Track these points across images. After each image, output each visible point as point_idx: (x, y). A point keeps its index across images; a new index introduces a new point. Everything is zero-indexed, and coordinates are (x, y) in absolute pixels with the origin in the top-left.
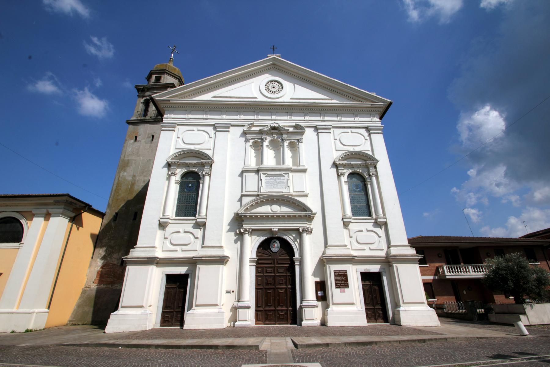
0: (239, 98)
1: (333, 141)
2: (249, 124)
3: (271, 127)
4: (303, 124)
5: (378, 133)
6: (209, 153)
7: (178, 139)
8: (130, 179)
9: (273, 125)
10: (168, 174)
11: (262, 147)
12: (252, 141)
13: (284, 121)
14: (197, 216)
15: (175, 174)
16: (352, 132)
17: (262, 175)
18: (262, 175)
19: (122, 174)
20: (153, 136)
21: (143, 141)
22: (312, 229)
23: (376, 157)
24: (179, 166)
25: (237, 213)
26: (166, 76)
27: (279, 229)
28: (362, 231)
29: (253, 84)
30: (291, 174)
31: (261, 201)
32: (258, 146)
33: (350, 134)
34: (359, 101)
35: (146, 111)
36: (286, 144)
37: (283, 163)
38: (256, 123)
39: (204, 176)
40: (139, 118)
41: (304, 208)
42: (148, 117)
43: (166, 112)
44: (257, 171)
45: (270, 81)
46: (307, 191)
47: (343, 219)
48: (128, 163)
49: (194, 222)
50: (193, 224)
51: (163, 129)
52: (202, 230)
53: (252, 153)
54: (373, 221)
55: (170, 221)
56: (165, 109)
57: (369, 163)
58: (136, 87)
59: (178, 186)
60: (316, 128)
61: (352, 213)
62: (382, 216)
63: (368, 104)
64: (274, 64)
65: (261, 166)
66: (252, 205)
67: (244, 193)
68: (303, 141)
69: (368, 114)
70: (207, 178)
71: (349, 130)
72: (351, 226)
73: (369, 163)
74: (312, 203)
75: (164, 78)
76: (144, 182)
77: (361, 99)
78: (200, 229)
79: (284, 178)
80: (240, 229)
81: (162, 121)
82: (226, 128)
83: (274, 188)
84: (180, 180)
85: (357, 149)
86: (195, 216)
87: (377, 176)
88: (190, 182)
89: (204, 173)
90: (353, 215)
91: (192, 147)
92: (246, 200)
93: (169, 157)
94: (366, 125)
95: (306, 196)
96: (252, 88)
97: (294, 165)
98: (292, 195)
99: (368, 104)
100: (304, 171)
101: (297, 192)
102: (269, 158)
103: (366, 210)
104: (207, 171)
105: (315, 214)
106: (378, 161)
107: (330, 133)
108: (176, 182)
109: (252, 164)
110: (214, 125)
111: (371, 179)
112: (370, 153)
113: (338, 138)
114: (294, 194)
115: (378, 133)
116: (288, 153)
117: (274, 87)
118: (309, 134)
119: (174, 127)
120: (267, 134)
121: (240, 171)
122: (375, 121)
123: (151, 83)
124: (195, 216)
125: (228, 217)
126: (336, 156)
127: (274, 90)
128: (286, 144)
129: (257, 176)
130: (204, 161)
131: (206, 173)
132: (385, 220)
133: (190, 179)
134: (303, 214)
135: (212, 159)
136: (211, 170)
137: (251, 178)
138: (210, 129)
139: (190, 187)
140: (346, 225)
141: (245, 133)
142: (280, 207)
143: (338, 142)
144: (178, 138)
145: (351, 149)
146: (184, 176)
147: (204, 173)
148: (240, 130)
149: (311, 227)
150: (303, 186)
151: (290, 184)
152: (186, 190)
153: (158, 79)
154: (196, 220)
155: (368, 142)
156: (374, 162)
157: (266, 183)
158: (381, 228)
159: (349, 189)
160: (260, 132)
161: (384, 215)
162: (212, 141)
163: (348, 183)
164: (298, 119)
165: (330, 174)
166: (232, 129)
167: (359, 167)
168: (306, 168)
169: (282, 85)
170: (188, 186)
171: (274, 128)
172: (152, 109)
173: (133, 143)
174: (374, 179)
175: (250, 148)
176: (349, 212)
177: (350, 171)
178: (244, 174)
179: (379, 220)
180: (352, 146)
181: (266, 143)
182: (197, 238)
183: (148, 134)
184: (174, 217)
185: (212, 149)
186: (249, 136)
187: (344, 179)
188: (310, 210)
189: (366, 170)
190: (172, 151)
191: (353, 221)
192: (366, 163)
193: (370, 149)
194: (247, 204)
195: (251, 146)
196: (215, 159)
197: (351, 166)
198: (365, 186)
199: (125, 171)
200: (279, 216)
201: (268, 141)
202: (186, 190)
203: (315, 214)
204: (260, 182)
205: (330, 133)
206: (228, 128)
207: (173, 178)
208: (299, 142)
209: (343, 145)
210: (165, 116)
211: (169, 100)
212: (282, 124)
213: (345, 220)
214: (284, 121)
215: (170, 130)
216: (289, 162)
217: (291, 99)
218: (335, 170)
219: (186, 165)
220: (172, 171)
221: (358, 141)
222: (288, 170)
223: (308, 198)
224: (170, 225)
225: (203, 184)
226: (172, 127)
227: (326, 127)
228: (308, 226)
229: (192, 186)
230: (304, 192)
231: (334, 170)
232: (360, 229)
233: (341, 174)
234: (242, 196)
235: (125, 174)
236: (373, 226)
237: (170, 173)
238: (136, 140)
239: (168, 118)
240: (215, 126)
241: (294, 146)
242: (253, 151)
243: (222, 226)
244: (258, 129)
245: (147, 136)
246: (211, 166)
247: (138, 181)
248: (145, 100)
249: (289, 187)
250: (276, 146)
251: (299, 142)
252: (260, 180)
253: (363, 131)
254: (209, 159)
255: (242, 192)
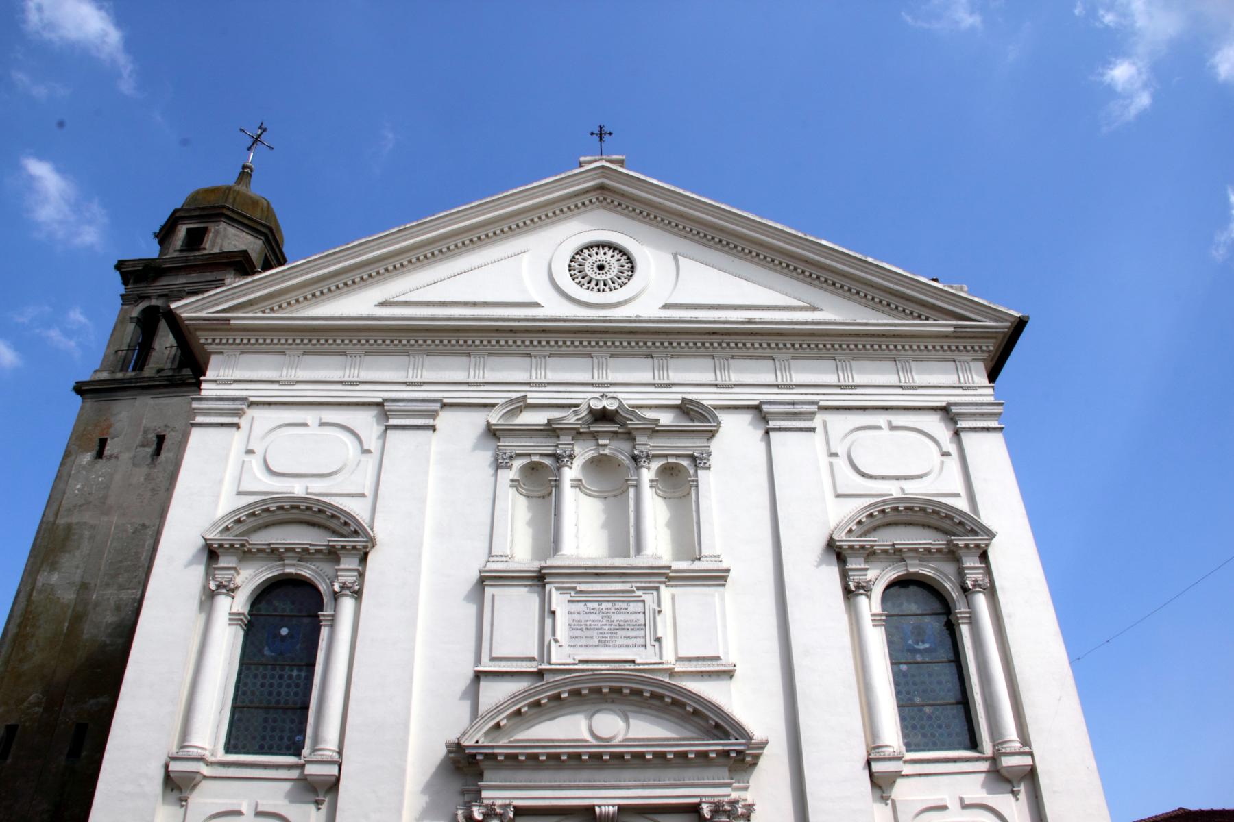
0: (474, 305)
1: (824, 460)
2: (511, 401)
3: (591, 411)
4: (708, 398)
5: (988, 429)
6: (358, 509)
7: (248, 458)
8: (68, 596)
9: (597, 405)
10: (205, 587)
11: (557, 484)
12: (518, 464)
13: (633, 385)
14: (306, 752)
15: (231, 591)
16: (893, 428)
17: (555, 594)
18: (555, 594)
19: (41, 579)
20: (161, 439)
21: (125, 457)
22: (750, 808)
23: (987, 518)
24: (246, 554)
25: (458, 745)
26: (222, 226)
27: (622, 809)
28: (944, 808)
29: (526, 257)
30: (666, 592)
31: (551, 698)
32: (541, 481)
33: (886, 432)
34: (919, 317)
35: (145, 347)
36: (648, 474)
37: (639, 550)
38: (534, 397)
39: (336, 596)
40: (119, 375)
41: (717, 724)
42: (148, 372)
43: (214, 360)
44: (539, 579)
45: (589, 247)
46: (731, 657)
47: (869, 763)
48: (67, 538)
49: (295, 774)
50: (287, 786)
51: (199, 419)
52: (324, 807)
53: (516, 511)
54: (984, 766)
55: (205, 770)
56: (210, 348)
57: (960, 541)
58: (120, 266)
59: (241, 633)
60: (759, 411)
61: (905, 736)
62: (1017, 745)
63: (945, 325)
64: (602, 188)
65: (550, 563)
66: (518, 713)
67: (487, 666)
68: (713, 461)
69: (945, 360)
70: (347, 604)
71: (881, 419)
72: (901, 790)
73: (960, 541)
74: (750, 704)
75: (217, 232)
76: (118, 608)
77: (917, 310)
78: (318, 803)
79: (639, 607)
80: (468, 807)
81: (198, 385)
82: (422, 415)
83: (603, 644)
84: (246, 610)
85: (915, 489)
86: (298, 754)
87: (991, 592)
88: (284, 619)
89: (337, 587)
90: (909, 747)
91: (298, 489)
92: (495, 694)
93: (215, 525)
94: (941, 401)
95: (729, 674)
96: (523, 274)
97: (678, 557)
98: (671, 673)
99: (945, 325)
100: (718, 578)
101: (690, 659)
102: (584, 530)
103: (958, 725)
104: (349, 578)
105: (763, 745)
106: (991, 535)
107: (813, 430)
108: (234, 618)
109: (520, 552)
110: (757, 409)
111: (970, 604)
112: (962, 504)
113: (841, 450)
114: (679, 668)
115: (988, 429)
116: (655, 510)
117: (601, 267)
118: (736, 438)
119: (239, 413)
120: (577, 434)
121: (475, 576)
122: (966, 382)
123: (172, 254)
124: (298, 754)
125: (421, 754)
126: (838, 516)
127: (601, 277)
128: (648, 474)
129: (534, 600)
130: (338, 542)
131: (344, 587)
132: (1027, 761)
133: (282, 605)
134: (714, 747)
135: (366, 534)
136: (361, 575)
137: (515, 611)
138: (365, 422)
139: (283, 638)
140: (881, 785)
141: (492, 433)
142: (626, 719)
143: (842, 464)
144: (250, 452)
145: (894, 490)
146: (264, 595)
147: (337, 587)
148: (478, 420)
149: (749, 797)
150: (717, 637)
151: (665, 630)
152: (266, 652)
153: (195, 239)
154: (302, 767)
155: (953, 464)
156: (980, 539)
157: (571, 627)
158: (1015, 794)
159: (890, 644)
160: (551, 430)
161: (1025, 741)
162: (370, 463)
163: (890, 620)
164: (692, 378)
165: (816, 584)
166: (445, 420)
167: (927, 554)
168: (724, 566)
169: (630, 260)
170: (277, 635)
171: (602, 416)
172: (165, 342)
173: (91, 464)
174: (981, 601)
175: (512, 491)
176: (891, 734)
177: (893, 574)
178: (489, 591)
179: (1007, 762)
180: (897, 478)
181: (570, 474)
182: (368, 452)
183: (146, 432)
184: (221, 756)
185: (369, 491)
186: (511, 445)
187: (870, 605)
188: (741, 732)
189: (949, 568)
190: (226, 504)
191: (907, 769)
192: (949, 542)
193: (959, 487)
194: (498, 709)
195: (515, 484)
196: (381, 531)
197: (896, 555)
198: (952, 629)
199: (53, 567)
200: (619, 757)
201: (578, 463)
202: (266, 652)
203: (763, 745)
204: (548, 622)
205: (813, 430)
206: (434, 414)
207: (225, 606)
208: (696, 467)
209: (863, 475)
210: (210, 374)
211: (228, 319)
212: (629, 398)
213: (877, 767)
214: (633, 385)
215: (222, 425)
216: (658, 546)
217: (666, 307)
218: (833, 572)
219: (274, 554)
220: (222, 577)
221: (912, 460)
222: (662, 576)
223: (734, 684)
224: (205, 784)
225: (332, 626)
226: (232, 413)
227: (798, 408)
228: (735, 795)
229: (290, 635)
230: (718, 658)
231: (832, 573)
232: (933, 798)
233: (858, 587)
234: (478, 676)
235: (55, 578)
236: (985, 785)
237: (212, 586)
238: (100, 455)
239: (223, 376)
240: (382, 408)
241: (678, 480)
242: (522, 502)
243: (401, 793)
244: (538, 418)
245: (139, 438)
246: (364, 558)
247: (97, 605)
248: (144, 311)
249: (658, 640)
250: (612, 478)
251: (696, 467)
252: (545, 602)
253: (935, 425)
254: (356, 533)
255: (478, 660)
